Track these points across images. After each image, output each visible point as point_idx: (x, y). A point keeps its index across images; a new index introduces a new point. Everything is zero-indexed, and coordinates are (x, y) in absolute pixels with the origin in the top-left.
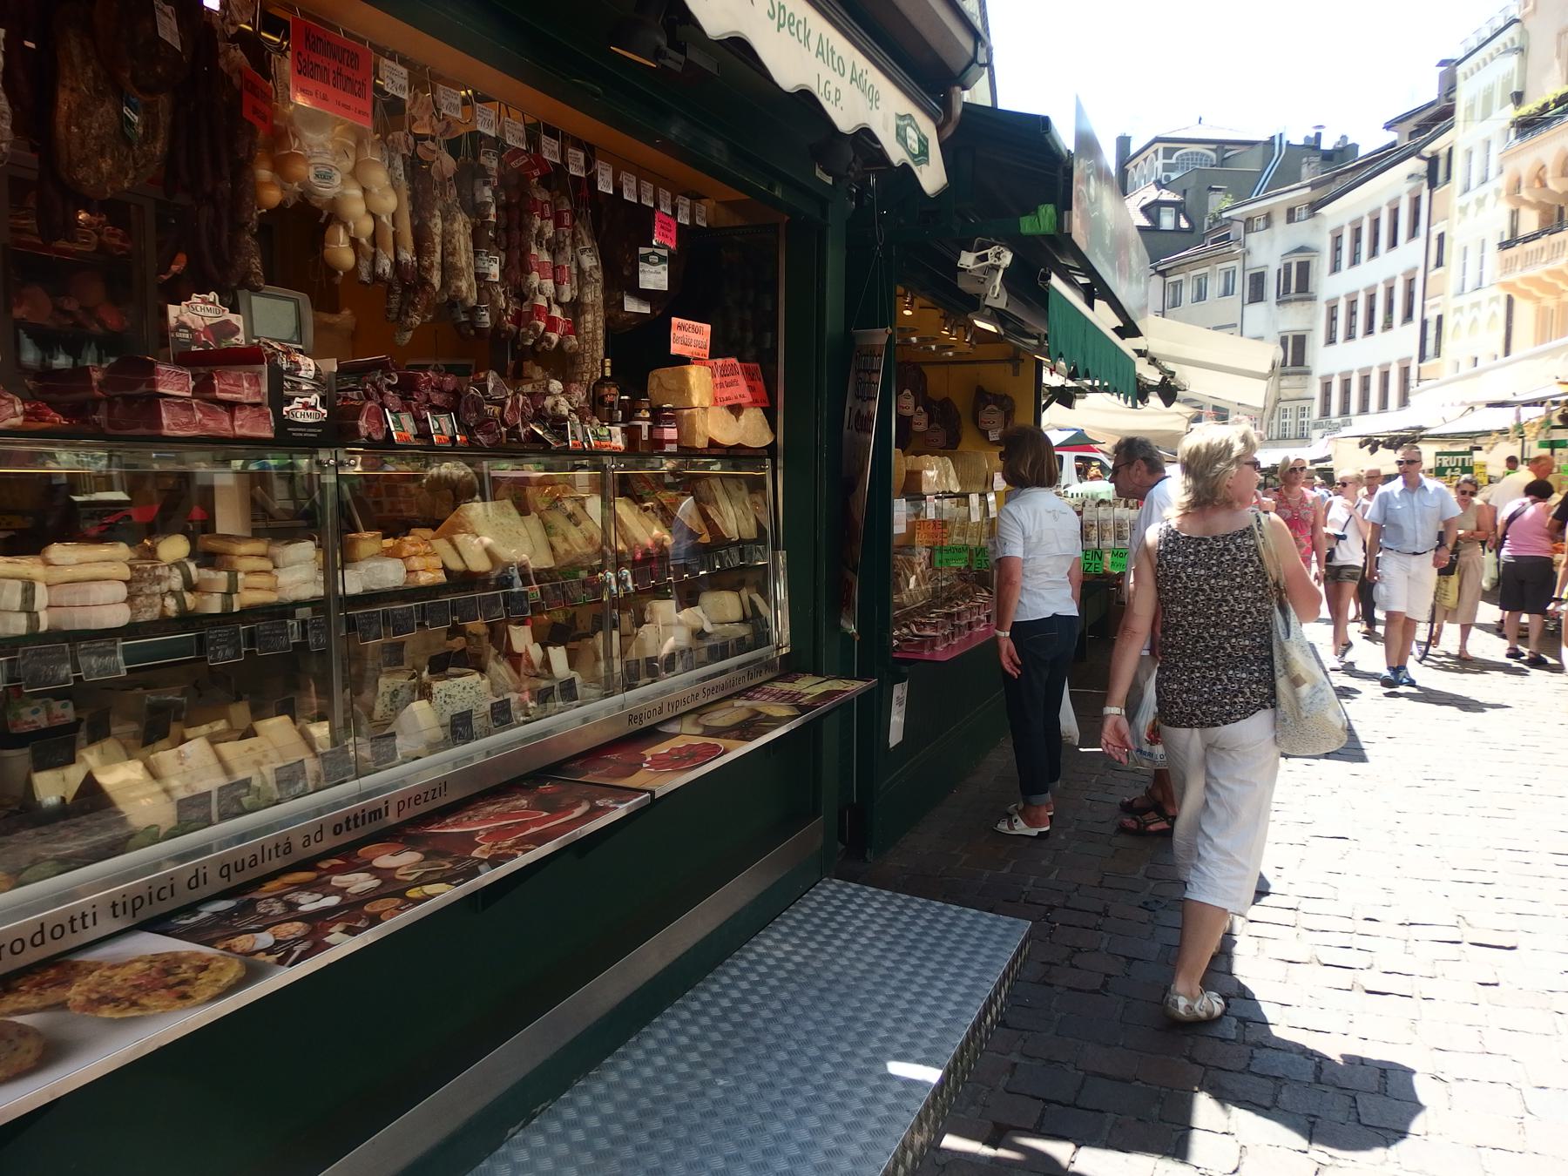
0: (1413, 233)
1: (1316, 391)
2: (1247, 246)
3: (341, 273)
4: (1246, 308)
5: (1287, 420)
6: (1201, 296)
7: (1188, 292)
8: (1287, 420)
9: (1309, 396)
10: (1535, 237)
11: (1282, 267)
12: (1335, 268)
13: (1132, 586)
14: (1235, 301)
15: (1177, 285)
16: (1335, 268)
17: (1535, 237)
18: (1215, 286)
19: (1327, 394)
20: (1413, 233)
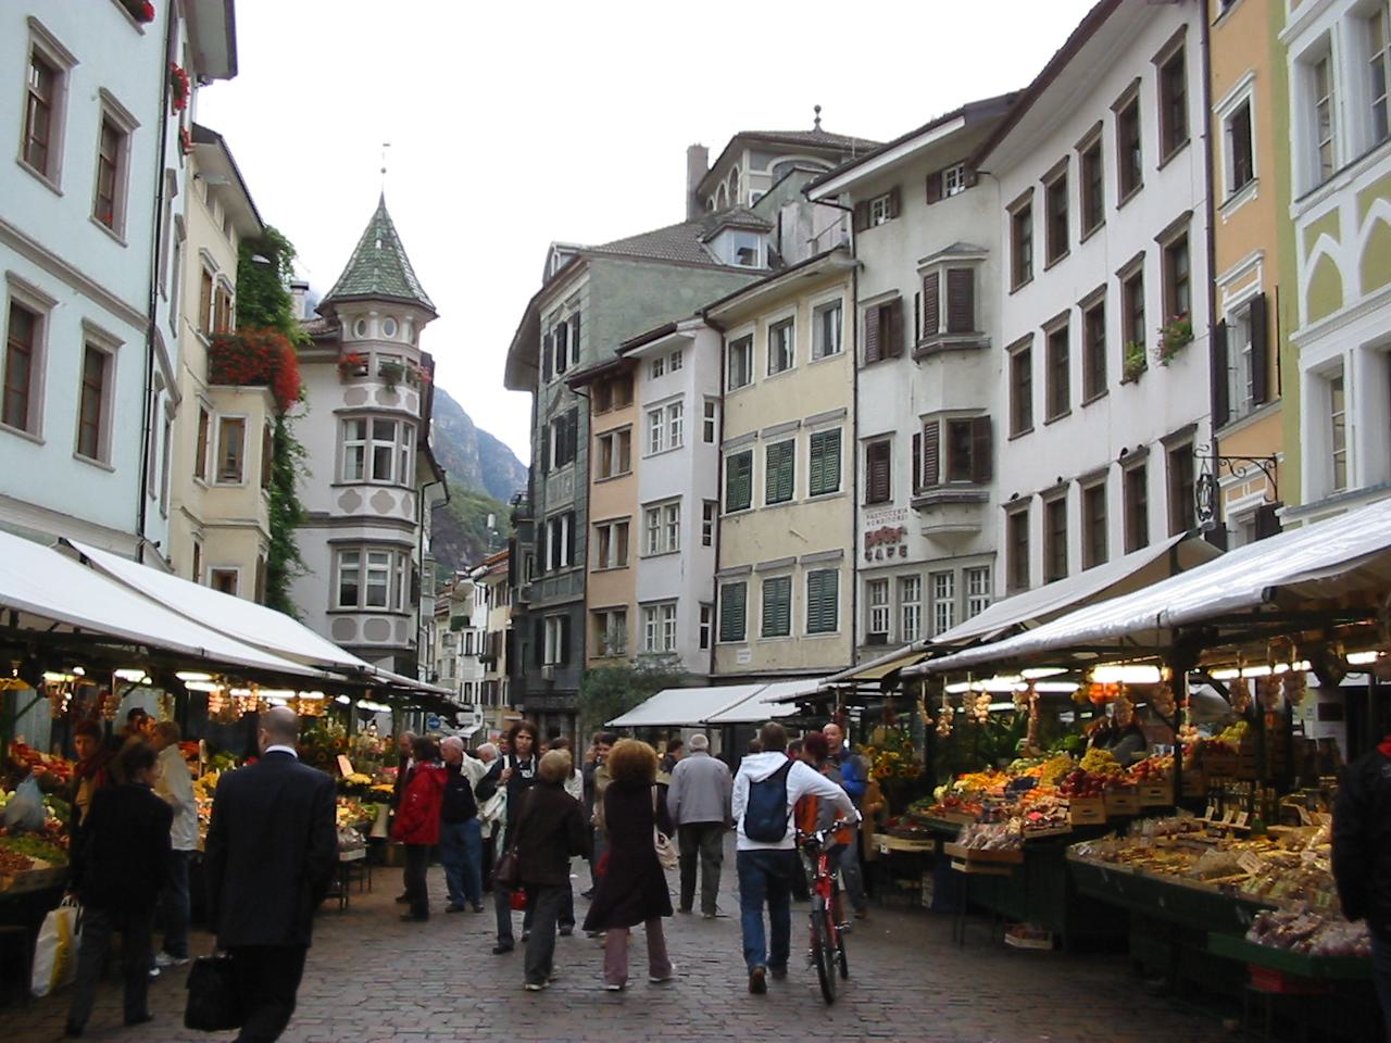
0: (1174, 136)
1: (997, 534)
2: (859, 256)
3: (15, 672)
4: (860, 376)
5: (947, 601)
6: (782, 361)
7: (761, 354)
8: (947, 601)
9: (985, 549)
10: (1246, 417)
11: (920, 430)
12: (1022, 274)
13: (499, 854)
14: (841, 366)
15: (743, 345)
16: (1022, 274)
17: (1246, 417)
18: (803, 340)
19: (1018, 522)
20: (1174, 136)
